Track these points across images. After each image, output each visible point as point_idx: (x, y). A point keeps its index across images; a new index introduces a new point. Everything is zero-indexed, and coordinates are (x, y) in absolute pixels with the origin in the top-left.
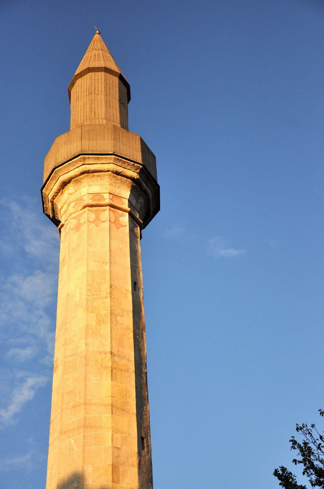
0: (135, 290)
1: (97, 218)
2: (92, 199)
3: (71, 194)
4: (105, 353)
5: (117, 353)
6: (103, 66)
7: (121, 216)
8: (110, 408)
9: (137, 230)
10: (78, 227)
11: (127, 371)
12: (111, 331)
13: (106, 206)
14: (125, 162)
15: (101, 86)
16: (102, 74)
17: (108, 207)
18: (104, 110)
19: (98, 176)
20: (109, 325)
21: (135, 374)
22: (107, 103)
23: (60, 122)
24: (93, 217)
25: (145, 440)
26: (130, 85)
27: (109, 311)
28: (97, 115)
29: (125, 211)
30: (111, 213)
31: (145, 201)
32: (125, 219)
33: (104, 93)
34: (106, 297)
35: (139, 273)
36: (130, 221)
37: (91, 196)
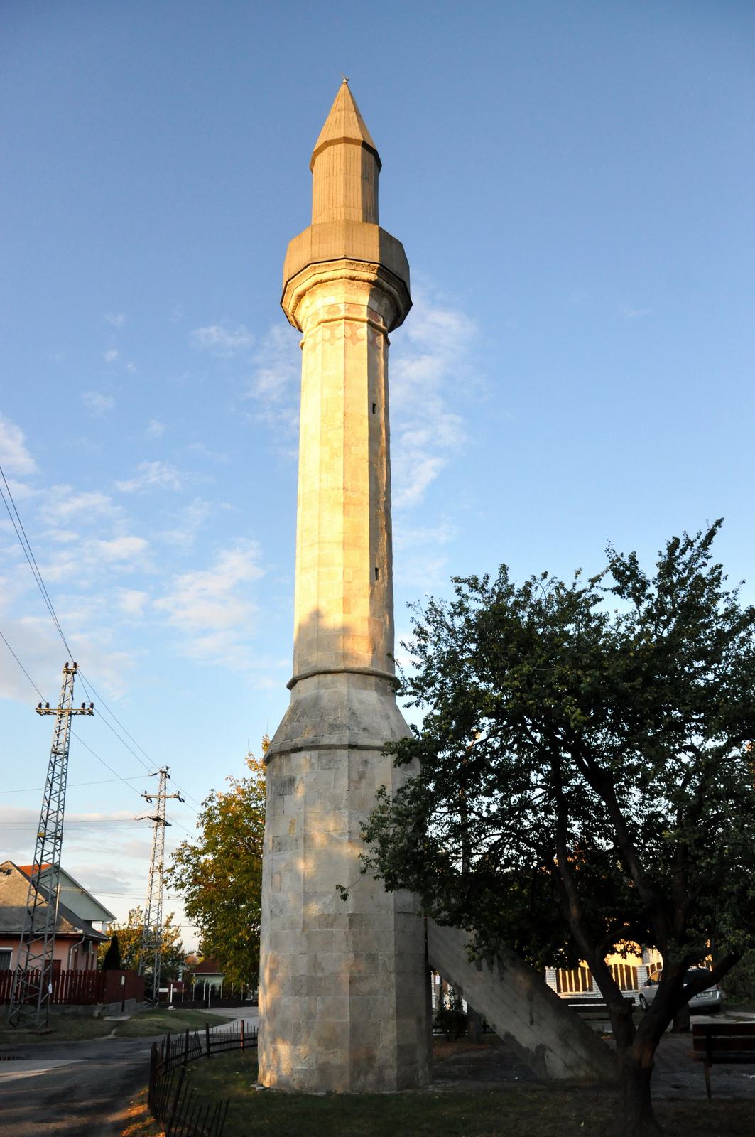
0: (374, 412)
1: (333, 336)
2: (328, 312)
3: (307, 308)
4: (338, 489)
5: (350, 488)
6: (342, 136)
7: (358, 328)
8: (341, 545)
9: (379, 339)
10: (314, 347)
11: (361, 504)
12: (344, 464)
13: (341, 319)
14: (359, 264)
15: (340, 164)
16: (341, 146)
17: (343, 321)
18: (342, 196)
19: (331, 285)
20: (342, 458)
21: (370, 507)
22: (347, 184)
23: (300, 218)
24: (328, 334)
25: (380, 571)
26: (377, 149)
27: (342, 443)
28: (334, 204)
29: (363, 321)
30: (348, 327)
31: (390, 302)
32: (363, 330)
33: (343, 172)
34: (340, 427)
35: (380, 391)
36: (370, 332)
37: (327, 308)
